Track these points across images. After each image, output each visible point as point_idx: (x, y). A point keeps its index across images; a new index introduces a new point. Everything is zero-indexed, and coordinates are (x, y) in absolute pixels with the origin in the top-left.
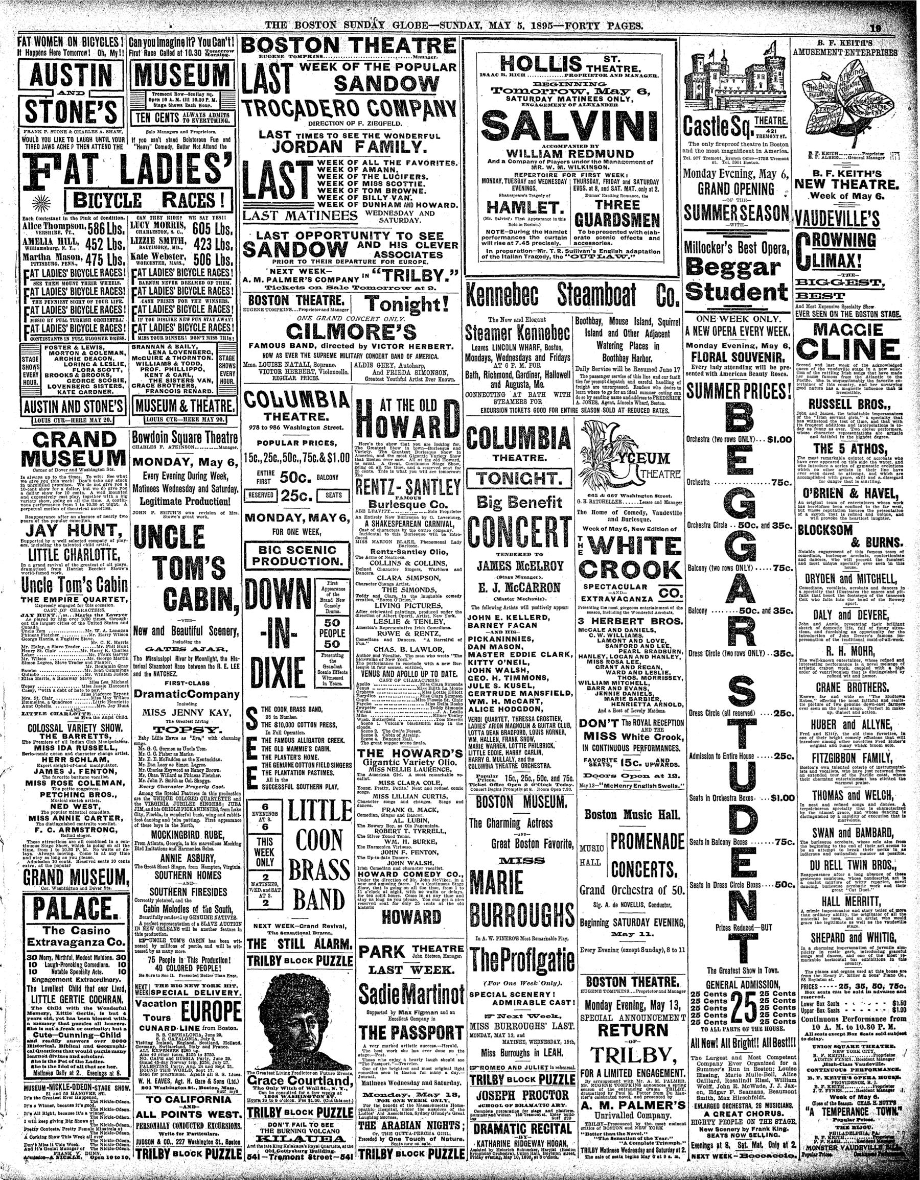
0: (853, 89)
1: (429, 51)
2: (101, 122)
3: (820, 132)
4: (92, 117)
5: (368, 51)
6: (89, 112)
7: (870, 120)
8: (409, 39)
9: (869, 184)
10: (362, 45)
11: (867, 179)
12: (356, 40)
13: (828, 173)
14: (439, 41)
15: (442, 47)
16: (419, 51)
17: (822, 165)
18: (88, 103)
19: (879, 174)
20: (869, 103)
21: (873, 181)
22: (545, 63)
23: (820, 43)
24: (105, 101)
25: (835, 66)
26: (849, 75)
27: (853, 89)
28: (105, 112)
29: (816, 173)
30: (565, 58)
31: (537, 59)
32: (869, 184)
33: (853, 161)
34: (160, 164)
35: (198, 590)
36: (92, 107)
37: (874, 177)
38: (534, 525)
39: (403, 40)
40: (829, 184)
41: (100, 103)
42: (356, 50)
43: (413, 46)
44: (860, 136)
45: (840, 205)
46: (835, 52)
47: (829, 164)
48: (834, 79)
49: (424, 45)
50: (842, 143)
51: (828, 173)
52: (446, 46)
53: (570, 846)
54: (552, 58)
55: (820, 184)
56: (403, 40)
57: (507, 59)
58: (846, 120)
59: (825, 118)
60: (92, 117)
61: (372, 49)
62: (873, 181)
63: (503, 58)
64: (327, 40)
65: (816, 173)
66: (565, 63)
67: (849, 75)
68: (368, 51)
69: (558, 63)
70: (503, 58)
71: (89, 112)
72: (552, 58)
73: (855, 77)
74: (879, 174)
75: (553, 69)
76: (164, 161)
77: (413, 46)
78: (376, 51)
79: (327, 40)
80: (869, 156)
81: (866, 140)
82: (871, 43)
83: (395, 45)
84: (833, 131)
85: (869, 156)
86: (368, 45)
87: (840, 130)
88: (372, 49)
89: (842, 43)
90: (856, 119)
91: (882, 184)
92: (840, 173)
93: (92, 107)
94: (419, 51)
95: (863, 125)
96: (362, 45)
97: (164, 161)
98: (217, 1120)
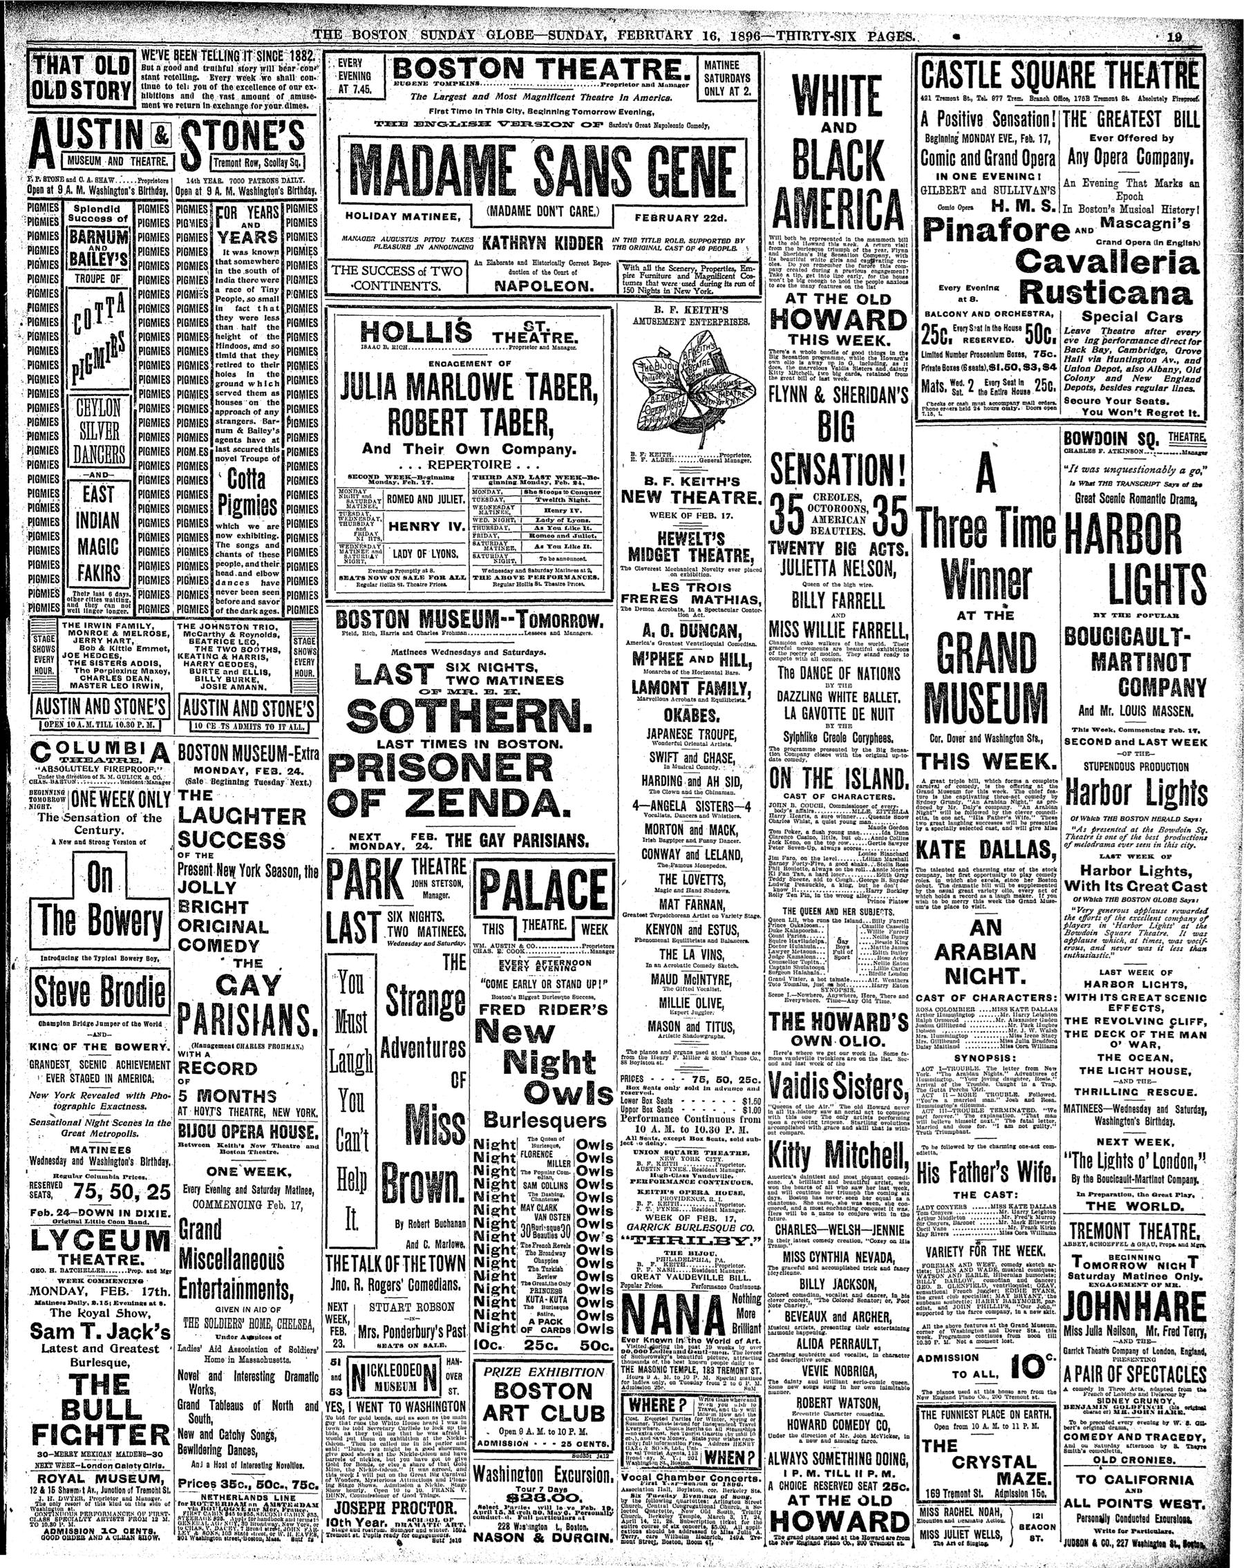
0: (700, 370)
1: (646, 77)
2: (284, 147)
3: (654, 428)
4: (272, 141)
5: (561, 76)
6: (269, 135)
7: (723, 411)
8: (616, 59)
9: (722, 497)
10: (554, 69)
11: (720, 490)
12: (546, 63)
13: (666, 480)
14: (658, 63)
15: (662, 71)
16: (631, 76)
17: (658, 471)
18: (267, 124)
19: (736, 482)
20: (723, 388)
21: (727, 493)
22: (420, 331)
23: (658, 310)
24: (288, 120)
25: (677, 339)
26: (694, 351)
27: (700, 370)
28: (287, 135)
29: (649, 481)
30: (449, 324)
31: (410, 324)
32: (722, 497)
33: (705, 465)
34: (416, 160)
35: (1110, 515)
36: (273, 129)
37: (729, 487)
38: (990, 692)
39: (609, 63)
40: (667, 497)
41: (282, 123)
42: (546, 76)
43: (622, 70)
44: (709, 433)
45: (681, 525)
46: (677, 322)
47: (658, 471)
48: (676, 356)
49: (639, 69)
50: (683, 444)
51: (666, 480)
52: (668, 69)
53: (310, 1327)
54: (429, 325)
55: (654, 496)
56: (609, 63)
57: (370, 326)
58: (691, 412)
59: (662, 408)
60: (272, 141)
61: (567, 74)
62: (727, 493)
63: (364, 324)
64: (508, 62)
65: (649, 481)
66: (449, 331)
67: (694, 351)
68: (561, 76)
69: (440, 331)
70: (364, 324)
71: (269, 135)
72: (429, 325)
73: (704, 354)
74: (736, 482)
75: (431, 339)
76: (423, 155)
77: (622, 70)
78: (573, 76)
79: (508, 62)
80: (730, 458)
81: (718, 440)
82: (726, 310)
83: (598, 68)
84: (674, 426)
85: (730, 458)
86: (562, 68)
87: (680, 424)
88: (567, 74)
89: (687, 311)
90: (704, 410)
91: (739, 497)
92: (684, 481)
93: (273, 129)
94: (631, 76)
95: (713, 418)
96: (554, 69)
97: (423, 155)
98: (1171, 1512)
